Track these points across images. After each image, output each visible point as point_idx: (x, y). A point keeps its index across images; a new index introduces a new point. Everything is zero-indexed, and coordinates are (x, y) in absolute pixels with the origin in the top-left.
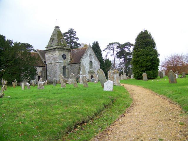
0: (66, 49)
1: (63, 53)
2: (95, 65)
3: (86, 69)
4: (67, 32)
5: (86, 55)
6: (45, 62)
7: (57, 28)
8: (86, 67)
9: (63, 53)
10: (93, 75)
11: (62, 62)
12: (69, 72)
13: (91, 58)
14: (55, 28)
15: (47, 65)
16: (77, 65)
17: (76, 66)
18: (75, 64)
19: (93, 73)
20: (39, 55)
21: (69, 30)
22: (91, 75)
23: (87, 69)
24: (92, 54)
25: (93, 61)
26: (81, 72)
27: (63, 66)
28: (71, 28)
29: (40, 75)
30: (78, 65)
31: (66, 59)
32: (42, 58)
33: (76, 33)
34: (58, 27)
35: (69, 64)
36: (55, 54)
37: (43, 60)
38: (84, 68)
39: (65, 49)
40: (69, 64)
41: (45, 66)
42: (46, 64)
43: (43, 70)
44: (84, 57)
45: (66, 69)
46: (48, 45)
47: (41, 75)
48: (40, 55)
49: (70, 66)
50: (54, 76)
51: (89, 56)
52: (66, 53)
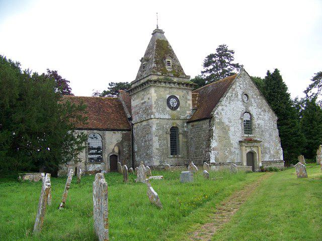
0: (179, 84)
1: (169, 93)
2: (259, 122)
3: (231, 134)
4: (215, 52)
5: (229, 94)
6: (131, 119)
7: (268, 71)
8: (232, 129)
9: (169, 93)
10: (255, 150)
11: (167, 117)
12: (187, 142)
13: (247, 104)
14: (153, 34)
15: (135, 126)
16: (205, 124)
17: (204, 126)
18: (201, 122)
19: (192, 149)
20: (121, 104)
21: (218, 50)
22: (249, 150)
23: (236, 133)
24: (250, 93)
25: (254, 110)
26: (214, 144)
27: (169, 127)
28: (221, 44)
29: (116, 150)
30: (208, 121)
31: (178, 109)
32: (126, 110)
33: (233, 53)
34: (161, 32)
35: (188, 123)
36: (148, 96)
37: (129, 116)
38: (225, 130)
39: (174, 83)
40: (188, 123)
41: (129, 130)
42: (133, 124)
43: (124, 138)
44: (224, 101)
45: (181, 136)
46: (138, 77)
47: (119, 151)
48: (123, 103)
49: (190, 126)
50: (147, 154)
51: (240, 97)
52: (179, 94)
